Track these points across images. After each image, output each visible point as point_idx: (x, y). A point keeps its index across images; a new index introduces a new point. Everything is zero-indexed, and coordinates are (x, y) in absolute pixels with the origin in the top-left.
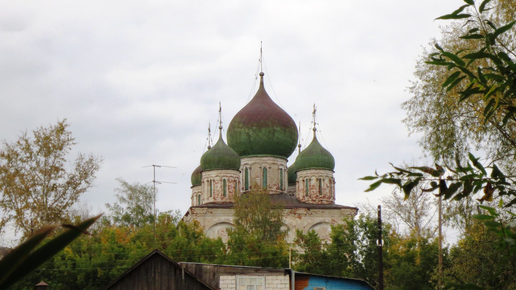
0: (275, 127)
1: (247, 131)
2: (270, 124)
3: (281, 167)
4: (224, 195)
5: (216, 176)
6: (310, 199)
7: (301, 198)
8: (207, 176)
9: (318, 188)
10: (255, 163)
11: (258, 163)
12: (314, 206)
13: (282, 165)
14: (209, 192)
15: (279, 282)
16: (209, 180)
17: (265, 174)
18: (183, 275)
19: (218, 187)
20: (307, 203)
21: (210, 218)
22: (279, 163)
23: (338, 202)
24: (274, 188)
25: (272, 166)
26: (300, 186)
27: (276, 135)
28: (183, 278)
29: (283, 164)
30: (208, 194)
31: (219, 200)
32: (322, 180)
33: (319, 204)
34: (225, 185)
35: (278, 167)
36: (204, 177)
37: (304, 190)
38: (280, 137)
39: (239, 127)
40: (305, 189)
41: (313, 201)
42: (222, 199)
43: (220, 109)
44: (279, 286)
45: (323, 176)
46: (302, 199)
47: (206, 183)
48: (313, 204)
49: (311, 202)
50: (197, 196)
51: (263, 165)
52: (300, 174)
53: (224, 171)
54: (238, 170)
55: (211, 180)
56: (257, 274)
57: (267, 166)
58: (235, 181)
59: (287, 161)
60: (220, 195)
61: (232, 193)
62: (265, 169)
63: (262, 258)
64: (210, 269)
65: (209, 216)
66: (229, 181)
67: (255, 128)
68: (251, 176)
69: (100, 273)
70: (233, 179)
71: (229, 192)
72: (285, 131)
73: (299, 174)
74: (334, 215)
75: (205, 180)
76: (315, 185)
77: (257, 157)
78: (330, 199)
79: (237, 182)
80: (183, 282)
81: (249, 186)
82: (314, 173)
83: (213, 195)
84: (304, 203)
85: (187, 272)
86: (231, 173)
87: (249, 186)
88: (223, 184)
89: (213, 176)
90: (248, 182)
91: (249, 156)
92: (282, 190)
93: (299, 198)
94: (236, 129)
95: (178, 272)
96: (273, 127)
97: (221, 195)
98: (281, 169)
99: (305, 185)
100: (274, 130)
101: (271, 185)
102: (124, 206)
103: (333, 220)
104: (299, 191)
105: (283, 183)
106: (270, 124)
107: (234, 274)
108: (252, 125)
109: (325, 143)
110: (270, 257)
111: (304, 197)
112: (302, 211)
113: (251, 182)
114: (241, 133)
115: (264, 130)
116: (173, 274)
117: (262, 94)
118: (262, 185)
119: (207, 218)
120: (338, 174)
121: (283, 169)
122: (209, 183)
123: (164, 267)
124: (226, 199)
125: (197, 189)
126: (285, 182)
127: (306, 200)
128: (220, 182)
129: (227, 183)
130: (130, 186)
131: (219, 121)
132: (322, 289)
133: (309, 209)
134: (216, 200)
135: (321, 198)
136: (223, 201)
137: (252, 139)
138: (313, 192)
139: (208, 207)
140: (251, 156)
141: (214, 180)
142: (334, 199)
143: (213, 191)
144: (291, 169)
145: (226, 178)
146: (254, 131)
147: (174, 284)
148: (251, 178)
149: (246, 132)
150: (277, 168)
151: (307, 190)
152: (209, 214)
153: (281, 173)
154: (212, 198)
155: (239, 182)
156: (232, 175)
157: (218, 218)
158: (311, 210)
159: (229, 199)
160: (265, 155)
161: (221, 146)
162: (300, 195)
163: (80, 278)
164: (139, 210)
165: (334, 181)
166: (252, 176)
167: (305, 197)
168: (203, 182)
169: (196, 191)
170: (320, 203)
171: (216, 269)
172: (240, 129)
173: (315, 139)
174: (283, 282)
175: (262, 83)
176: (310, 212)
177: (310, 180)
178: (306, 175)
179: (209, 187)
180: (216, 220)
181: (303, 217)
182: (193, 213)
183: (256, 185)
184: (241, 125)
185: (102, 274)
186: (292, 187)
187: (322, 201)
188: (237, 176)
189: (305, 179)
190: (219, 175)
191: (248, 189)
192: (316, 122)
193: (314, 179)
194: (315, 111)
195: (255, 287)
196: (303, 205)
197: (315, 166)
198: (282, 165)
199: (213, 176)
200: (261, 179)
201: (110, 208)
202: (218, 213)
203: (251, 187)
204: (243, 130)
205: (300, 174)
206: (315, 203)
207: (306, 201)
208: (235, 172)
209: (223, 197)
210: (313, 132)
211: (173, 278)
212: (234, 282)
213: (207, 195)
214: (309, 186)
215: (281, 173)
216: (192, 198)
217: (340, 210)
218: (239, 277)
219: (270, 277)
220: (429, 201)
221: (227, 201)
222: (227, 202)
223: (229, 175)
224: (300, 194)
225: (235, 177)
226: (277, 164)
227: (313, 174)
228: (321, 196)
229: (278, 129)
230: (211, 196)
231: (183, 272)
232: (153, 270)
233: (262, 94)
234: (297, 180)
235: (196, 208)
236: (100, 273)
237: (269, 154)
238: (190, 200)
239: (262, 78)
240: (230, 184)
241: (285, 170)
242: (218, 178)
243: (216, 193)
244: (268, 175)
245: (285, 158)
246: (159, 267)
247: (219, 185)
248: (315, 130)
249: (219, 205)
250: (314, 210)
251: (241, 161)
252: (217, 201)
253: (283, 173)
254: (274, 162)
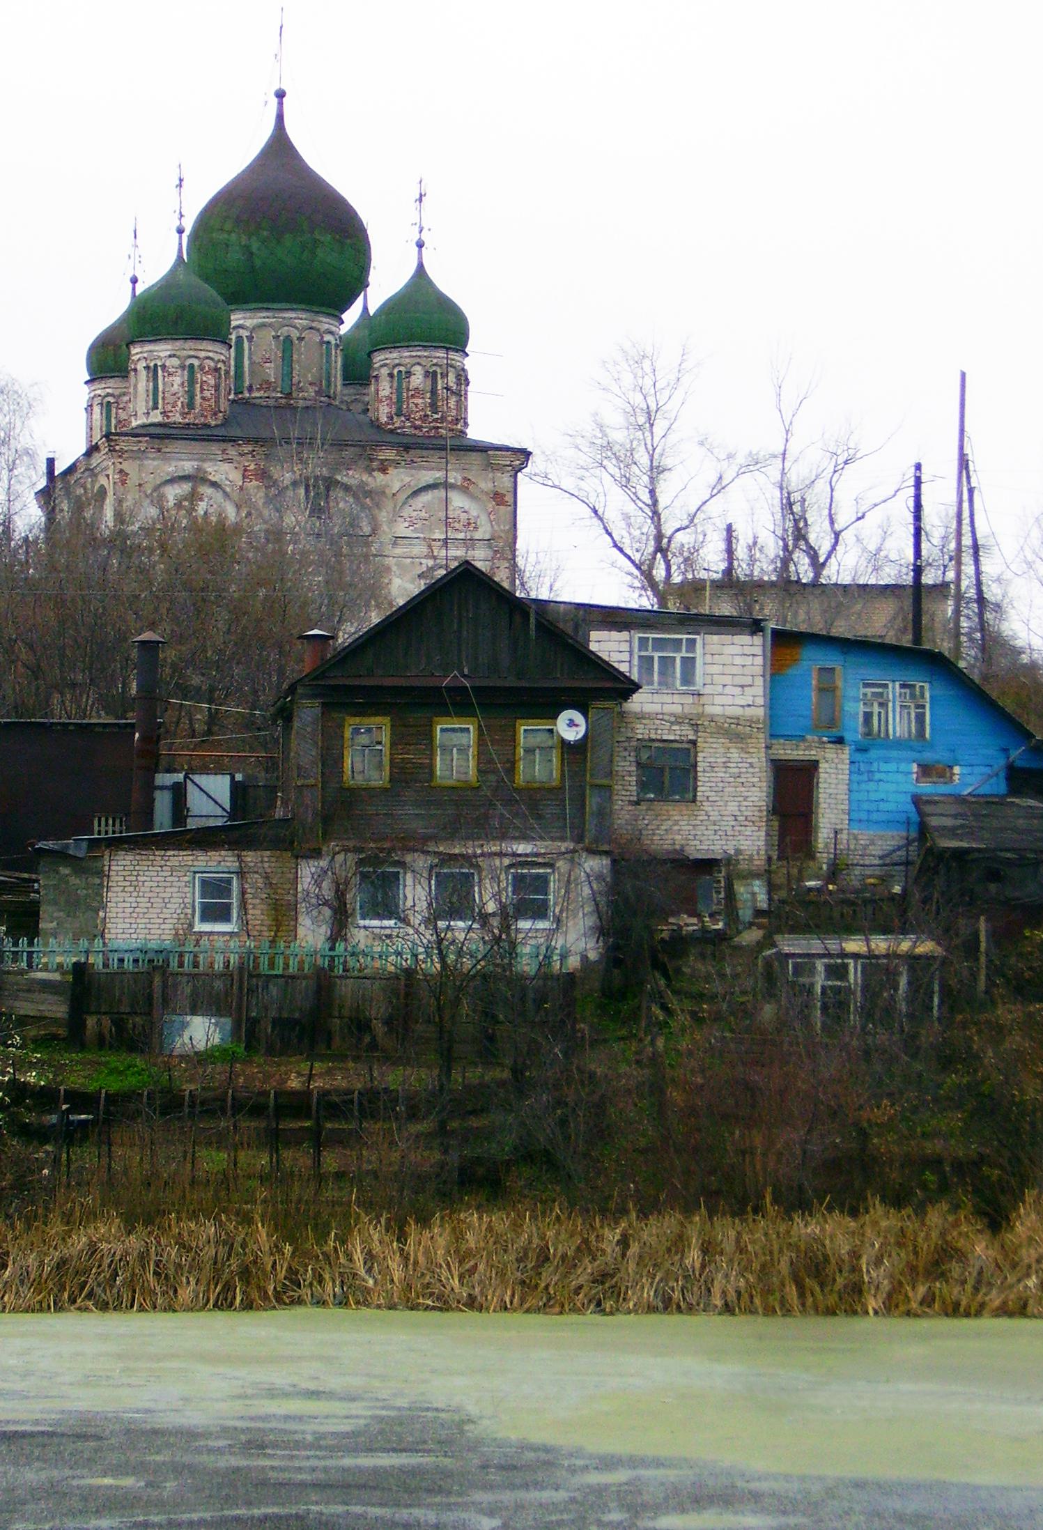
0: (316, 233)
2: (305, 226)
3: (327, 338)
4: (191, 405)
5: (170, 356)
6: (408, 424)
7: (384, 419)
8: (145, 355)
9: (428, 395)
10: (263, 325)
11: (271, 325)
13: (331, 333)
14: (151, 397)
15: (736, 650)
16: (152, 365)
17: (287, 354)
20: (398, 434)
21: (156, 463)
23: (475, 432)
24: (311, 391)
26: (381, 388)
28: (533, 633)
29: (334, 329)
30: (147, 402)
32: (439, 376)
33: (430, 437)
34: (192, 381)
35: (322, 337)
36: (138, 356)
37: (391, 399)
41: (416, 428)
42: (183, 415)
44: (738, 660)
45: (440, 366)
47: (143, 374)
50: (101, 404)
51: (285, 331)
52: (382, 357)
53: (190, 344)
55: (156, 365)
57: (295, 334)
58: (217, 370)
59: (342, 322)
61: (209, 400)
65: (154, 459)
66: (202, 370)
67: (265, 233)
68: (250, 358)
71: (203, 398)
74: (467, 466)
75: (141, 366)
77: (268, 309)
78: (457, 424)
81: (247, 384)
82: (419, 357)
83: (160, 406)
84: (392, 432)
85: (543, 621)
86: (210, 351)
87: (247, 384)
88: (186, 378)
89: (162, 354)
91: (244, 306)
92: (329, 397)
93: (378, 419)
94: (214, 235)
97: (183, 406)
98: (328, 343)
99: (395, 384)
100: (316, 241)
101: (301, 384)
103: (465, 479)
106: (305, 226)
109: (446, 282)
111: (392, 418)
112: (388, 454)
113: (252, 372)
114: (227, 246)
117: (280, 146)
118: (280, 382)
119: (145, 462)
120: (474, 362)
121: (333, 342)
125: (104, 386)
126: (336, 377)
128: (179, 371)
131: (178, 212)
132: (833, 669)
133: (407, 448)
134: (168, 417)
135: (436, 420)
137: (258, 262)
138: (416, 405)
140: (253, 306)
141: (164, 367)
142: (466, 424)
143: (161, 395)
144: (346, 344)
145: (196, 363)
148: (252, 363)
149: (243, 243)
151: (400, 401)
153: (329, 355)
154: (158, 412)
156: (211, 354)
157: (174, 463)
158: (412, 452)
160: (288, 306)
161: (181, 277)
165: (467, 379)
167: (395, 417)
168: (135, 370)
169: (99, 392)
173: (421, 267)
174: (748, 650)
175: (280, 118)
176: (408, 457)
178: (397, 361)
180: (170, 469)
182: (112, 450)
183: (267, 385)
184: (228, 226)
189: (395, 372)
190: (178, 353)
191: (242, 393)
192: (423, 225)
194: (181, 180)
196: (389, 438)
198: (331, 333)
200: (276, 368)
202: (177, 450)
203: (250, 389)
204: (234, 237)
205: (382, 357)
206: (421, 434)
207: (396, 428)
208: (217, 347)
209: (186, 410)
210: (417, 249)
212: (625, 647)
213: (144, 403)
216: (89, 408)
217: (484, 454)
219: (715, 637)
221: (197, 422)
222: (197, 425)
223: (203, 354)
224: (381, 408)
225: (219, 361)
226: (318, 330)
227: (418, 360)
228: (436, 416)
231: (532, 620)
233: (280, 146)
235: (123, 438)
237: (288, 299)
239: (281, 104)
240: (204, 379)
242: (176, 362)
245: (336, 313)
247: (177, 380)
248: (420, 245)
250: (419, 451)
251: (232, 318)
252: (172, 420)
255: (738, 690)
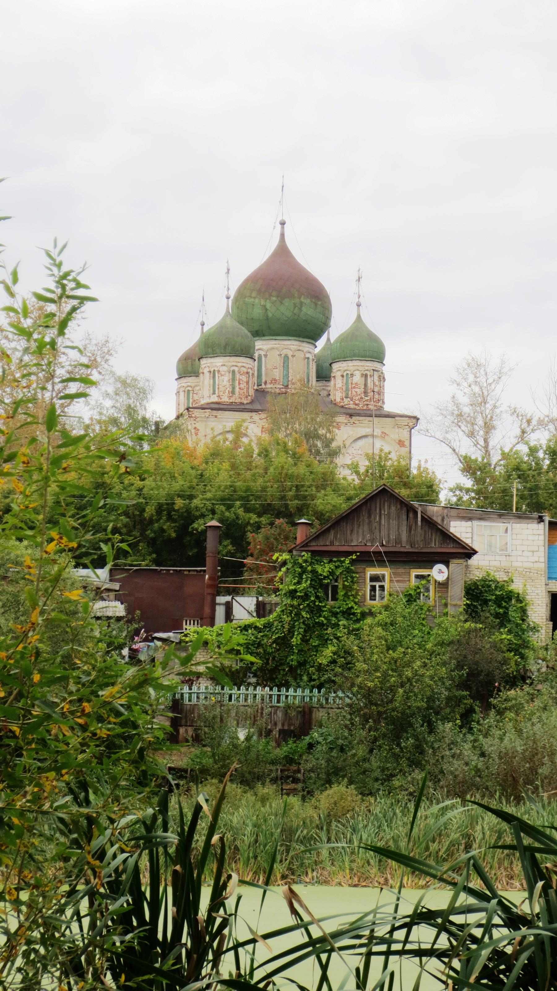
1: (263, 302)
2: (296, 295)
3: (308, 355)
4: (233, 392)
6: (351, 402)
7: (338, 400)
9: (363, 387)
10: (273, 349)
11: (277, 349)
12: (357, 412)
16: (212, 370)
17: (286, 365)
18: (419, 519)
19: (224, 381)
22: (306, 349)
23: (388, 407)
25: (297, 354)
27: (304, 309)
28: (419, 523)
29: (311, 350)
30: (209, 390)
31: (225, 399)
34: (233, 379)
38: (309, 313)
39: (250, 296)
40: (344, 389)
41: (356, 405)
42: (230, 397)
43: (228, 270)
44: (530, 537)
46: (340, 402)
47: (207, 375)
48: (355, 409)
49: (352, 406)
51: (284, 352)
54: (252, 358)
55: (214, 371)
56: (501, 520)
57: (290, 353)
59: (316, 347)
60: (227, 391)
62: (286, 357)
63: (414, 490)
64: (437, 512)
65: (213, 422)
67: (274, 298)
68: (266, 367)
69: (179, 503)
70: (245, 370)
71: (240, 388)
72: (316, 304)
73: (335, 366)
75: (206, 371)
76: (359, 382)
79: (251, 374)
80: (419, 528)
81: (263, 381)
83: (217, 392)
84: (342, 407)
86: (243, 362)
87: (263, 381)
89: (218, 364)
90: (261, 375)
91: (264, 338)
94: (246, 299)
95: (411, 515)
96: (300, 298)
98: (308, 358)
100: (301, 303)
102: (108, 403)
103: (383, 432)
104: (335, 389)
105: (310, 378)
107: (470, 519)
108: (271, 295)
110: (424, 490)
111: (343, 399)
114: (253, 305)
115: (287, 302)
116: (405, 517)
121: (311, 358)
122: (212, 375)
123: (393, 508)
124: (236, 399)
127: (346, 403)
128: (227, 374)
129: (237, 376)
130: (120, 377)
133: (351, 416)
134: (221, 399)
135: (367, 401)
136: (231, 401)
137: (270, 315)
139: (212, 409)
141: (219, 371)
142: (383, 402)
143: (217, 387)
145: (236, 369)
146: (273, 303)
147: (405, 532)
148: (266, 369)
150: (303, 356)
151: (347, 389)
152: (213, 419)
153: (308, 363)
154: (215, 396)
155: (253, 374)
156: (244, 365)
158: (354, 418)
159: (240, 398)
162: (337, 396)
163: (150, 510)
164: (130, 411)
165: (384, 378)
166: (268, 366)
168: (203, 373)
169: (183, 385)
170: (365, 408)
171: (446, 511)
172: (253, 300)
173: (359, 317)
174: (536, 532)
175: (282, 235)
177: (352, 375)
178: (346, 368)
179: (212, 381)
181: (342, 427)
184: (254, 295)
185: (182, 505)
186: (320, 384)
187: (368, 405)
188: (250, 366)
189: (345, 374)
190: (226, 364)
193: (358, 374)
195: (498, 537)
196: (343, 410)
197: (359, 357)
199: (218, 364)
201: (90, 406)
203: (266, 383)
206: (358, 408)
211: (406, 522)
212: (469, 530)
214: (350, 384)
215: (308, 363)
217: (393, 419)
218: (476, 523)
219: (518, 525)
220: (500, 409)
223: (239, 365)
224: (337, 394)
228: (367, 398)
229: (307, 301)
230: (214, 393)
232: (378, 511)
234: (332, 375)
236: (179, 503)
238: (175, 397)
239: (283, 228)
241: (313, 360)
243: (222, 389)
244: (290, 366)
245: (313, 342)
246: (386, 507)
248: (359, 305)
249: (226, 407)
250: (358, 418)
252: (223, 400)
253: (311, 363)
254: (299, 348)
255: (531, 554)
